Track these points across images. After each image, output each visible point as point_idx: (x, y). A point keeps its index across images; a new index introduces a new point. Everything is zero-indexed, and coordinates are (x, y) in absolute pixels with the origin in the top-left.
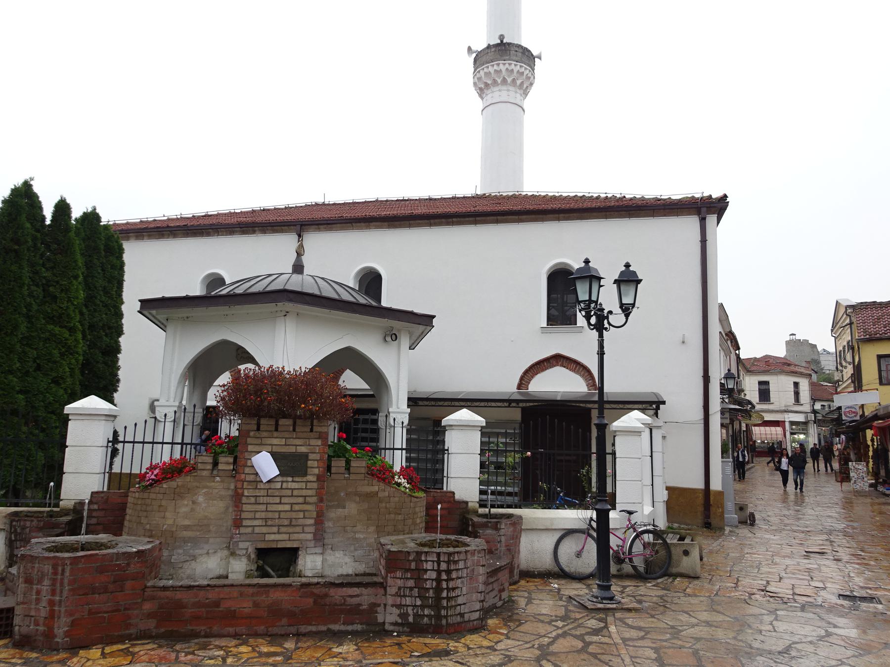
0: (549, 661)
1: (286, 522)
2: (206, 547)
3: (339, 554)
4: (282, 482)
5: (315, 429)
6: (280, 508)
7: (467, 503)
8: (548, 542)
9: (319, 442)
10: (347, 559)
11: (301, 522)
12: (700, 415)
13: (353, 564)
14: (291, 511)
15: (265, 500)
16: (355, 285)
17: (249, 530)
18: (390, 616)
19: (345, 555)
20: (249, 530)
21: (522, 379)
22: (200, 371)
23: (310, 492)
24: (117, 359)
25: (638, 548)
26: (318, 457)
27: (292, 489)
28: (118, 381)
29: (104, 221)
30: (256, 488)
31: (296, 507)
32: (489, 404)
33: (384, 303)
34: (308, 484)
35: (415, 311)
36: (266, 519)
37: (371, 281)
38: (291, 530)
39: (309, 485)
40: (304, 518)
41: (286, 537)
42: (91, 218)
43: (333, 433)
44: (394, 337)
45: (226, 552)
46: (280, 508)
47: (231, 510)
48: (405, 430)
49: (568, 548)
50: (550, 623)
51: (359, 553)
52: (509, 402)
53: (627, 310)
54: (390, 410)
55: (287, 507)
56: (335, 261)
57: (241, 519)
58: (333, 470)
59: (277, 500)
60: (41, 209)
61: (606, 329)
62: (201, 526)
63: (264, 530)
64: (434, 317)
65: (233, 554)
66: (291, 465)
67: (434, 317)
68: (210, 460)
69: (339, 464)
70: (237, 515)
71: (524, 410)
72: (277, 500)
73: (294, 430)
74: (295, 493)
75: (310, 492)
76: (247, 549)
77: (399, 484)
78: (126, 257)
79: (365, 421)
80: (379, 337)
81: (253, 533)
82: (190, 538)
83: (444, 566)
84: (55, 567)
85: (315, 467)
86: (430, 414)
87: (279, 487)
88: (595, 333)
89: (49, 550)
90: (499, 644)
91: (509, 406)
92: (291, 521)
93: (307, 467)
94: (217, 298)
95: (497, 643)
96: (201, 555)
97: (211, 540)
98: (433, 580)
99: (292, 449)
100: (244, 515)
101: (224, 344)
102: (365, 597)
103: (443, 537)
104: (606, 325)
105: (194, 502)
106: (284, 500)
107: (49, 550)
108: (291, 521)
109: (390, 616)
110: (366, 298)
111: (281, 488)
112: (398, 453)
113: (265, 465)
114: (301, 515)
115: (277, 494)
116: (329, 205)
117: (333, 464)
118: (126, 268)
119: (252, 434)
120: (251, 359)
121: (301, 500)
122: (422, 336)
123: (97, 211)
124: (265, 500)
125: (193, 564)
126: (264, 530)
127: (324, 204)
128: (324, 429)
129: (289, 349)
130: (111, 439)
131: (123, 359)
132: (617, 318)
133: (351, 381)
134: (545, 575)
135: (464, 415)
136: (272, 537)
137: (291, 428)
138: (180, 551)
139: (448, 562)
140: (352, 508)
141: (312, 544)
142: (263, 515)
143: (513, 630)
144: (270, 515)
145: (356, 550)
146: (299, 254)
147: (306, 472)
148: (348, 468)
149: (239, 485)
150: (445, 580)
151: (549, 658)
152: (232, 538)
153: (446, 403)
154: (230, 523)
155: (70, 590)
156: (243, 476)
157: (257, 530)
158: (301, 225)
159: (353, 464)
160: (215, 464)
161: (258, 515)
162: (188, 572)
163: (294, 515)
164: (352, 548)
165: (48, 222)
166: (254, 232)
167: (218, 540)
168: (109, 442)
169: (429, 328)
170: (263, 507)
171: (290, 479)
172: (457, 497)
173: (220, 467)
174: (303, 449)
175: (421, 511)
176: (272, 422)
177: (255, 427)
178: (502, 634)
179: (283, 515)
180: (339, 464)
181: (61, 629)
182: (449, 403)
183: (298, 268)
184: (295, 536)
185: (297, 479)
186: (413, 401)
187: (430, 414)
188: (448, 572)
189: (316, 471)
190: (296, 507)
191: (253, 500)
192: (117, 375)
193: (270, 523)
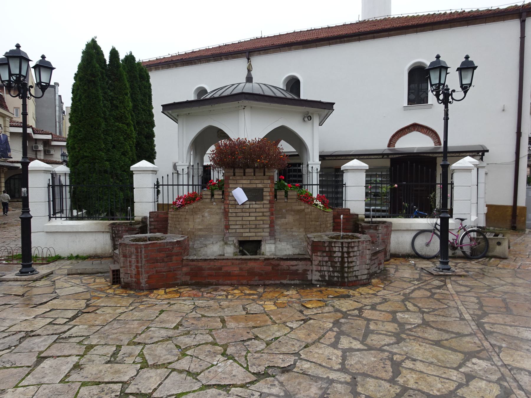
0: (410, 302)
2: (212, 240)
4: (250, 204)
5: (266, 174)
6: (250, 218)
7: (357, 215)
8: (408, 238)
12: (513, 158)
14: (256, 220)
15: (241, 214)
18: (315, 277)
22: (199, 145)
23: (265, 210)
24: (153, 141)
25: (467, 240)
30: (236, 208)
31: (259, 218)
32: (370, 157)
33: (302, 97)
35: (322, 101)
36: (242, 225)
37: (294, 84)
38: (256, 230)
41: (254, 234)
42: (130, 58)
44: (309, 118)
45: (222, 243)
46: (250, 218)
47: (223, 220)
49: (420, 242)
50: (410, 282)
51: (295, 243)
52: (382, 155)
53: (465, 88)
55: (254, 218)
56: (272, 73)
60: (103, 55)
61: (450, 102)
63: (242, 231)
64: (334, 104)
65: (226, 243)
66: (254, 195)
67: (334, 104)
68: (209, 193)
69: (281, 194)
71: (392, 160)
73: (254, 175)
74: (257, 210)
75: (265, 210)
77: (317, 205)
78: (151, 81)
80: (299, 119)
81: (236, 232)
83: (345, 249)
84: (137, 249)
86: (332, 167)
88: (442, 106)
91: (383, 158)
94: (203, 101)
95: (378, 292)
97: (214, 236)
99: (254, 186)
100: (230, 223)
102: (300, 266)
103: (345, 234)
104: (450, 100)
105: (203, 216)
106: (252, 214)
109: (315, 277)
111: (250, 208)
113: (239, 195)
114: (262, 222)
115: (247, 211)
116: (264, 38)
117: (278, 194)
118: (152, 87)
119: (231, 178)
121: (261, 214)
124: (241, 214)
125: (206, 249)
126: (242, 231)
127: (261, 38)
129: (248, 128)
132: (458, 94)
133: (285, 147)
134: (406, 257)
135: (355, 163)
136: (247, 234)
137: (253, 174)
138: (199, 242)
139: (348, 247)
140: (290, 218)
141: (269, 238)
142: (240, 223)
144: (244, 223)
145: (293, 241)
146: (249, 71)
151: (409, 300)
152: (225, 235)
153: (343, 158)
154: (223, 227)
156: (228, 202)
157: (238, 231)
158: (249, 52)
159: (289, 193)
160: (212, 195)
162: (204, 253)
163: (257, 222)
164: (291, 241)
165: (108, 63)
166: (221, 59)
167: (218, 236)
168: (155, 185)
169: (331, 111)
170: (240, 218)
171: (254, 203)
172: (351, 212)
173: (215, 197)
174: (260, 186)
177: (232, 174)
179: (251, 223)
181: (143, 280)
183: (249, 79)
184: (259, 234)
185: (258, 203)
186: (322, 157)
187: (332, 167)
188: (348, 253)
189: (268, 198)
190: (259, 218)
193: (244, 227)
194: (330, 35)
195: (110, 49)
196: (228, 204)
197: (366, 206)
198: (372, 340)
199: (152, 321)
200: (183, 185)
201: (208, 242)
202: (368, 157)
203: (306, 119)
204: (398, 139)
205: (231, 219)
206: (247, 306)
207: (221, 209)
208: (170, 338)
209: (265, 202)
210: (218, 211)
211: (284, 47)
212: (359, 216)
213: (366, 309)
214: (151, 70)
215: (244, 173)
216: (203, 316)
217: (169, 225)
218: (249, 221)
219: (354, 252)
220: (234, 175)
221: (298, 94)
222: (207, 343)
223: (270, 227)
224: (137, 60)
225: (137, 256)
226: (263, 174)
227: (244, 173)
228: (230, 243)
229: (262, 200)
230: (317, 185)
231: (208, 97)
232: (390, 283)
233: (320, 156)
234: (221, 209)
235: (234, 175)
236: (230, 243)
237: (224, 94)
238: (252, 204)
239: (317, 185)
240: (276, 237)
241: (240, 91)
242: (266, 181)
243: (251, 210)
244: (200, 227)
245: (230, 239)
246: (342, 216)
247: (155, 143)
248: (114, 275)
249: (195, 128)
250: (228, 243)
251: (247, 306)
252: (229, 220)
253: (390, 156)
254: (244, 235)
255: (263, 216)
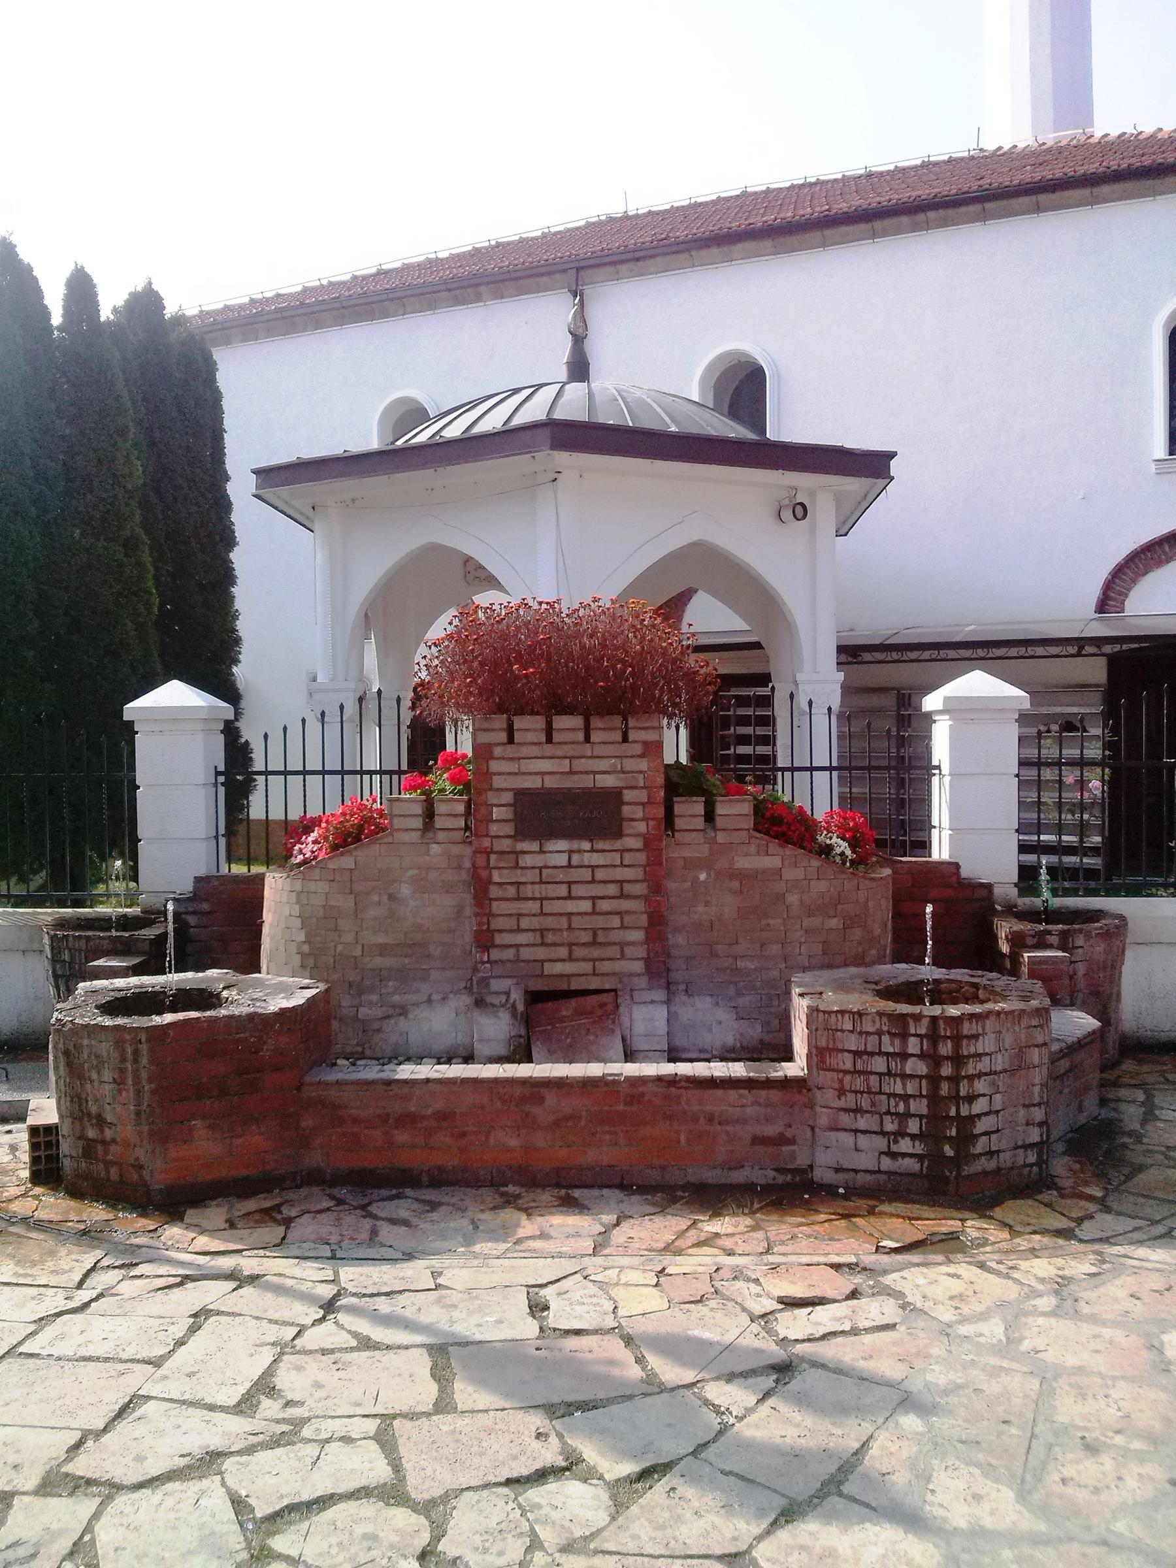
1: (586, 937)
2: (425, 988)
3: (703, 1003)
4: (571, 852)
5: (632, 735)
6: (571, 906)
7: (989, 887)
9: (643, 765)
10: (723, 1015)
11: (615, 936)
13: (736, 1025)
14: (594, 913)
15: (538, 891)
16: (703, 393)
17: (509, 954)
19: (717, 1004)
20: (509, 954)
21: (1108, 586)
22: (386, 613)
24: (230, 599)
26: (643, 796)
27: (593, 868)
28: (238, 641)
29: (170, 309)
30: (517, 866)
31: (604, 905)
32: (1031, 651)
33: (771, 434)
34: (627, 855)
36: (542, 931)
37: (743, 386)
38: (596, 953)
39: (628, 858)
40: (623, 927)
41: (586, 967)
42: (146, 303)
43: (676, 745)
44: (799, 510)
45: (466, 1000)
46: (571, 906)
47: (468, 912)
48: (834, 718)
51: (746, 1000)
52: (1080, 645)
54: (799, 677)
55: (586, 906)
56: (660, 349)
57: (491, 932)
58: (679, 823)
59: (562, 890)
60: (38, 293)
62: (410, 946)
63: (541, 953)
64: (892, 455)
65: (480, 1003)
67: (892, 455)
69: (690, 810)
70: (480, 924)
71: (1114, 662)
72: (562, 890)
73: (587, 739)
74: (600, 874)
75: (629, 874)
76: (508, 994)
77: (828, 849)
78: (223, 380)
79: (743, 701)
81: (517, 960)
82: (390, 969)
83: (946, 1070)
84: (119, 1044)
85: (638, 821)
86: (888, 676)
87: (565, 863)
89: (109, 1008)
90: (1086, 1225)
91: (1079, 654)
92: (595, 936)
93: (621, 820)
94: (411, 457)
95: (1080, 1221)
96: (417, 1005)
97: (435, 975)
98: (921, 1077)
99: (585, 782)
100: (496, 924)
101: (434, 553)
103: (939, 973)
105: (392, 898)
106: (578, 890)
107: (109, 1008)
108: (595, 936)
110: (737, 427)
111: (570, 866)
112: (822, 778)
114: (616, 921)
115: (561, 877)
116: (637, 216)
117: (678, 809)
118: (225, 404)
119: (498, 751)
120: (491, 582)
121: (612, 889)
122: (865, 503)
123: (155, 287)
124: (538, 891)
125: (402, 1023)
126: (541, 953)
127: (626, 217)
128: (650, 736)
129: (564, 557)
130: (221, 768)
131: (244, 596)
133: (709, 617)
135: (977, 683)
136: (558, 968)
137: (580, 736)
138: (375, 998)
139: (957, 1039)
141: (643, 982)
142: (535, 922)
143: (1117, 1189)
144: (550, 922)
145: (739, 994)
146: (579, 340)
147: (620, 827)
148: (710, 816)
149: (481, 861)
150: (947, 1078)
152: (475, 970)
153: (927, 655)
154: (468, 938)
155: (153, 1092)
156: (486, 842)
157: (526, 953)
158: (578, 269)
159: (721, 809)
161: (525, 923)
162: (394, 1038)
163: (600, 922)
164: (731, 990)
165: (56, 319)
166: (478, 298)
167: (448, 973)
168: (218, 773)
169: (881, 482)
170: (534, 906)
171: (586, 845)
174: (609, 781)
175: (881, 911)
176: (539, 722)
177: (503, 737)
178: (1090, 1198)
179: (576, 922)
180: (690, 810)
182: (934, 654)
183: (579, 369)
184: (606, 967)
185: (600, 845)
186: (850, 654)
187: (888, 676)
188: (958, 1060)
189: (641, 827)
190: (604, 905)
191: (511, 891)
192: (234, 630)
193: (550, 938)
194: (872, 200)
195: (67, 274)
196: (488, 853)
197: (1020, 852)
198: (1064, 1481)
199: (156, 1363)
200: (323, 773)
201: (414, 998)
202: (1022, 651)
203: (787, 514)
204: (1134, 581)
205: (496, 907)
206: (548, 1293)
207: (460, 867)
208: (208, 1462)
209: (631, 842)
210: (450, 876)
211: (708, 246)
212: (998, 891)
213: (1036, 1312)
214: (227, 341)
215: (549, 731)
216: (366, 1344)
217: (26, 1158)
218: (570, 915)
219: (978, 1056)
220: (511, 740)
221: (757, 420)
222: (361, 1493)
223: (648, 940)
224: (170, 310)
225: (122, 1071)
226: (618, 737)
227: (549, 731)
228: (495, 1000)
229: (619, 834)
230: (830, 769)
231: (422, 438)
232: (1129, 1178)
233: (841, 649)
234: (460, 867)
235: (511, 740)
236: (495, 1000)
237: (479, 429)
238: (579, 851)
239: (830, 769)
240: (675, 976)
241: (541, 416)
242: (629, 764)
243: (576, 875)
244: (381, 939)
245: (496, 985)
246: (929, 909)
247: (238, 604)
248: (34, 1146)
249: (378, 557)
250: (489, 999)
251: (548, 1293)
252: (490, 915)
253: (1108, 649)
254: (550, 969)
255: (622, 896)
